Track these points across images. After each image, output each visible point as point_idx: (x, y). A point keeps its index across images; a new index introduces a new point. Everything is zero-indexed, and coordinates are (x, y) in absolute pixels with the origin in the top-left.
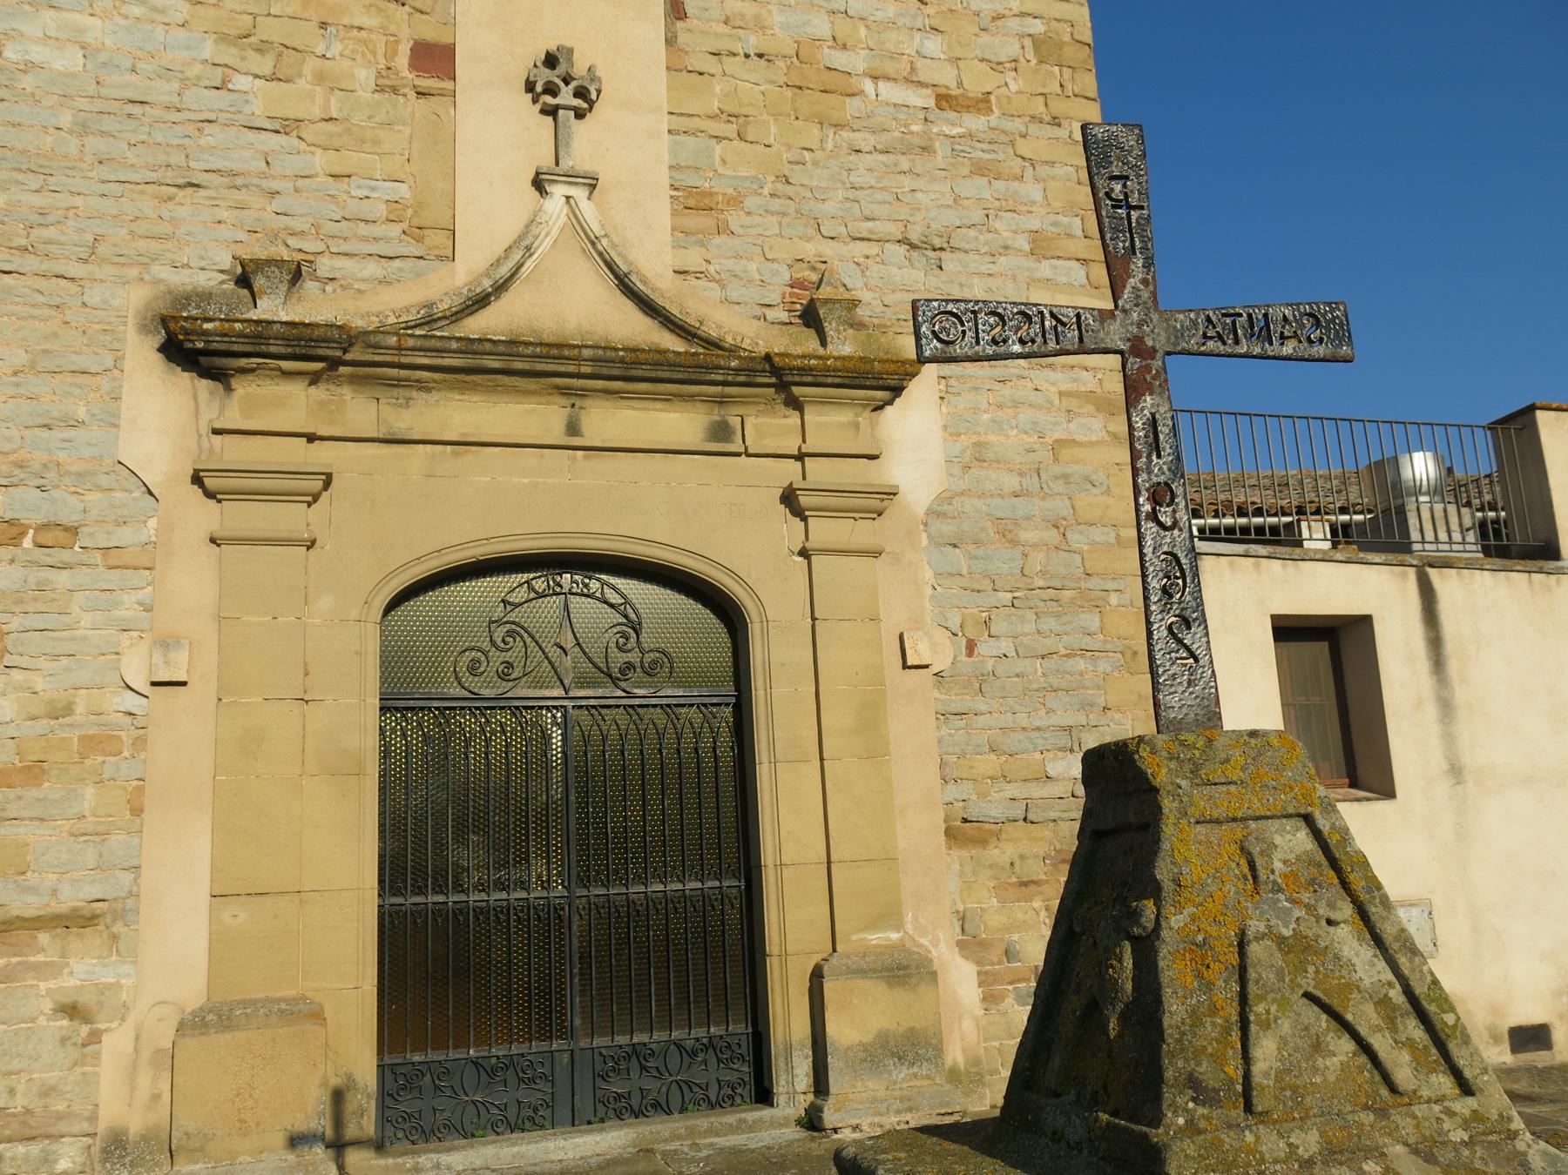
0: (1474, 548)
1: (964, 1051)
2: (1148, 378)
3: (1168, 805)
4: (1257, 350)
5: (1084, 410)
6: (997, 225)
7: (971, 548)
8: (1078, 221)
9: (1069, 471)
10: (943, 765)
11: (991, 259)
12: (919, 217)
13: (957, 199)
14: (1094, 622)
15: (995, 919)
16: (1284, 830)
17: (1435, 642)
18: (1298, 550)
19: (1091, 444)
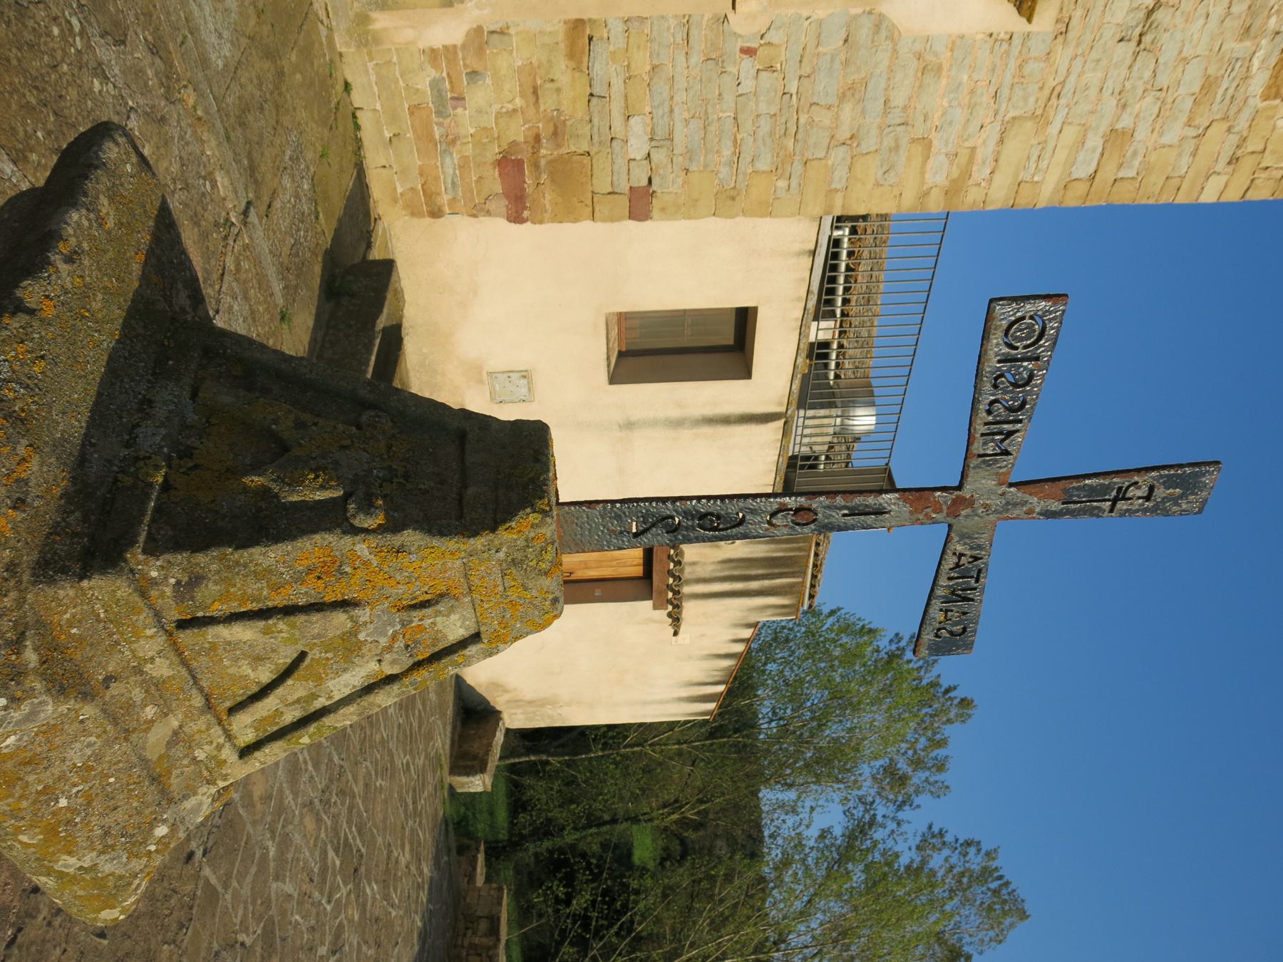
0: (797, 450)
1: (385, 29)
2: (929, 510)
3: (479, 542)
4: (940, 592)
5: (955, 167)
6: (1149, 99)
7: (842, 57)
8: (1132, 174)
9: (901, 151)
10: (642, 19)
11: (1117, 91)
12: (1179, 20)
13: (1186, 61)
14: (764, 164)
15: (503, 63)
16: (465, 620)
17: (727, 420)
18: (811, 317)
19: (923, 172)
